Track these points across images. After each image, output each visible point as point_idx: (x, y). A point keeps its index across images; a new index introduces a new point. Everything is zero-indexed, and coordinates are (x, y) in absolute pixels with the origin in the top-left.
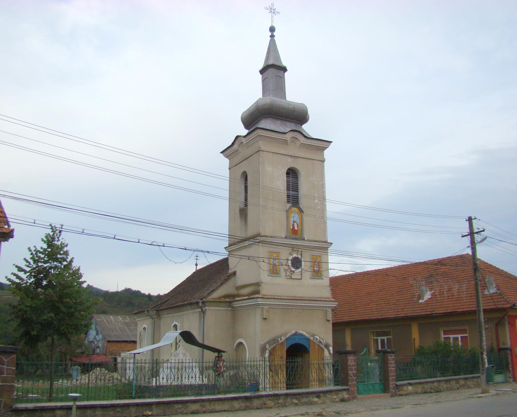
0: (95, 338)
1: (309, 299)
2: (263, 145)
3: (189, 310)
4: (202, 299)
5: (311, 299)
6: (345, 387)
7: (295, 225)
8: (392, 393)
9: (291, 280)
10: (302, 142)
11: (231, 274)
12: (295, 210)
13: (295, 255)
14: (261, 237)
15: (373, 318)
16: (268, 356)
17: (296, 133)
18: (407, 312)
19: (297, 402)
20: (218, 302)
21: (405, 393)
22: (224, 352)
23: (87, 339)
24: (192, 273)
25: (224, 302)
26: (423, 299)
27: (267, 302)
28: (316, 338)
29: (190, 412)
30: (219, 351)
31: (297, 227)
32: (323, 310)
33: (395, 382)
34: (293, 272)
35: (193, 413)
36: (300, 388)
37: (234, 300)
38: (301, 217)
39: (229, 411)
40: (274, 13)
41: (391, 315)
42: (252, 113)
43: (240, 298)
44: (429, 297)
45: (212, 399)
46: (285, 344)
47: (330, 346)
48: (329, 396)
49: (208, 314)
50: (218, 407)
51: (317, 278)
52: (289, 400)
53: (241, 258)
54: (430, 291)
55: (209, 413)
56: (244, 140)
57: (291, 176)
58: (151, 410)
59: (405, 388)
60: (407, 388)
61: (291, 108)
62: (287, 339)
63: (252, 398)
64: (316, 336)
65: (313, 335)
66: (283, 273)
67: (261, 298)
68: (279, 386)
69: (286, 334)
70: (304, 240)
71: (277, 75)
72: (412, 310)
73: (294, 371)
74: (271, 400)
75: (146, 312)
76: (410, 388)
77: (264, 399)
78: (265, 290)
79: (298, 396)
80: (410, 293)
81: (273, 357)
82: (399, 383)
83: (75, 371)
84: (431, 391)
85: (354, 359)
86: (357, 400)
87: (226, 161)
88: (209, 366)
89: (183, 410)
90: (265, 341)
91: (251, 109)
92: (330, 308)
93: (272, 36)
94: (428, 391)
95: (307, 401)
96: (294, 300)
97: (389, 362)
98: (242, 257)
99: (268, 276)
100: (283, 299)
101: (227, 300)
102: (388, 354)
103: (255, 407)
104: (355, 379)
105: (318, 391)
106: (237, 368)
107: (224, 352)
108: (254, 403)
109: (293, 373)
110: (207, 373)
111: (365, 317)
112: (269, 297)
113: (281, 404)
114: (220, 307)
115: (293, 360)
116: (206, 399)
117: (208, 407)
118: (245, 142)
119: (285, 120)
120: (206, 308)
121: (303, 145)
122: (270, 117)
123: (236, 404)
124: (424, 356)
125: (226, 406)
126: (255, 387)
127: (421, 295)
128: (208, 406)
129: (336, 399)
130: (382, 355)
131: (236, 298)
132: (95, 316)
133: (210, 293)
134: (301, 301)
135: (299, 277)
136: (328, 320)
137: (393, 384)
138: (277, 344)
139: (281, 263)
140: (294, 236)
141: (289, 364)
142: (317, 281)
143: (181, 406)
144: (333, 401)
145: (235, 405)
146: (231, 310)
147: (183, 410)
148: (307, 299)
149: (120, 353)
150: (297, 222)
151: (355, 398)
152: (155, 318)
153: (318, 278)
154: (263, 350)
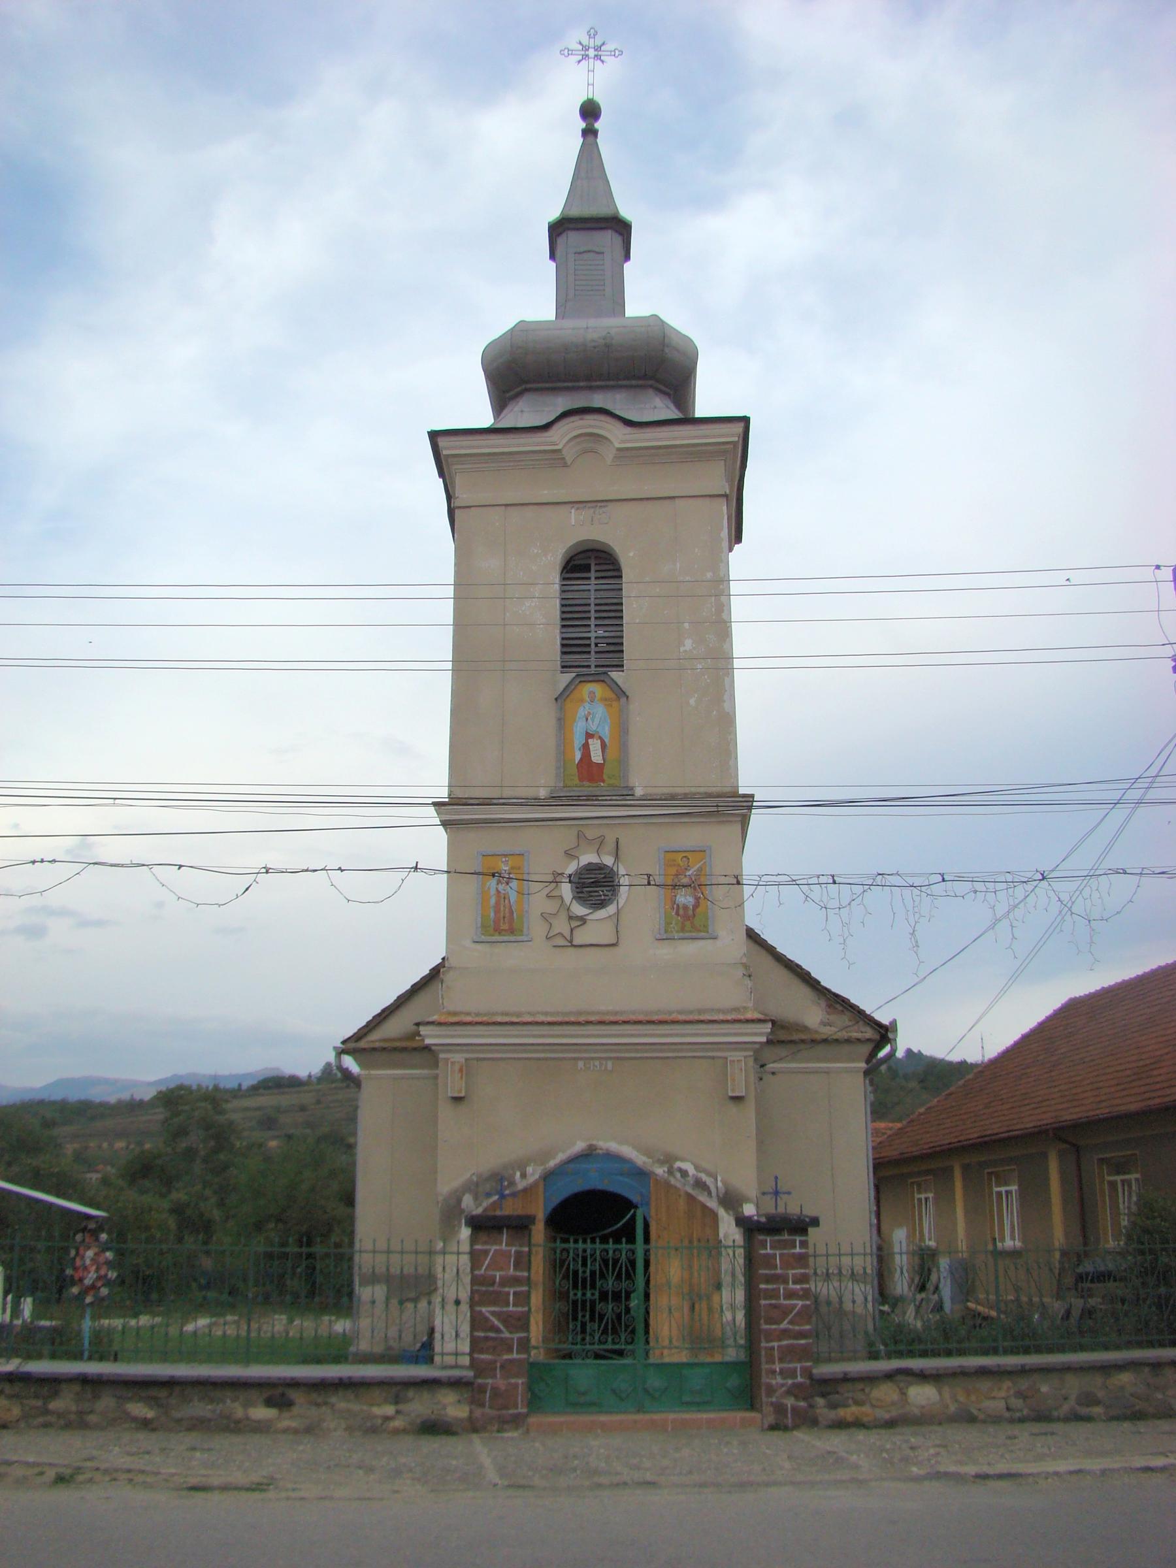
5: (655, 1018)
8: (780, 1409)
9: (572, 950)
10: (617, 445)
13: (588, 858)
17: (596, 417)
19: (150, 1414)
20: (404, 1049)
27: (453, 1036)
28: (680, 1170)
32: (713, 1058)
34: (583, 920)
47: (748, 1200)
48: (341, 1402)
51: (687, 935)
52: (107, 1402)
61: (593, 341)
62: (548, 1177)
64: (683, 1160)
65: (668, 1159)
66: (537, 929)
76: (922, 1395)
79: (163, 1393)
84: (1083, 1411)
85: (518, 1253)
92: (745, 1050)
95: (209, 1415)
99: (474, 942)
113: (60, 1415)
114: (413, 1067)
119: (590, 388)
121: (625, 455)
129: (387, 1418)
136: (737, 1099)
140: (588, 789)
142: (690, 949)
151: (516, 1421)
153: (694, 934)
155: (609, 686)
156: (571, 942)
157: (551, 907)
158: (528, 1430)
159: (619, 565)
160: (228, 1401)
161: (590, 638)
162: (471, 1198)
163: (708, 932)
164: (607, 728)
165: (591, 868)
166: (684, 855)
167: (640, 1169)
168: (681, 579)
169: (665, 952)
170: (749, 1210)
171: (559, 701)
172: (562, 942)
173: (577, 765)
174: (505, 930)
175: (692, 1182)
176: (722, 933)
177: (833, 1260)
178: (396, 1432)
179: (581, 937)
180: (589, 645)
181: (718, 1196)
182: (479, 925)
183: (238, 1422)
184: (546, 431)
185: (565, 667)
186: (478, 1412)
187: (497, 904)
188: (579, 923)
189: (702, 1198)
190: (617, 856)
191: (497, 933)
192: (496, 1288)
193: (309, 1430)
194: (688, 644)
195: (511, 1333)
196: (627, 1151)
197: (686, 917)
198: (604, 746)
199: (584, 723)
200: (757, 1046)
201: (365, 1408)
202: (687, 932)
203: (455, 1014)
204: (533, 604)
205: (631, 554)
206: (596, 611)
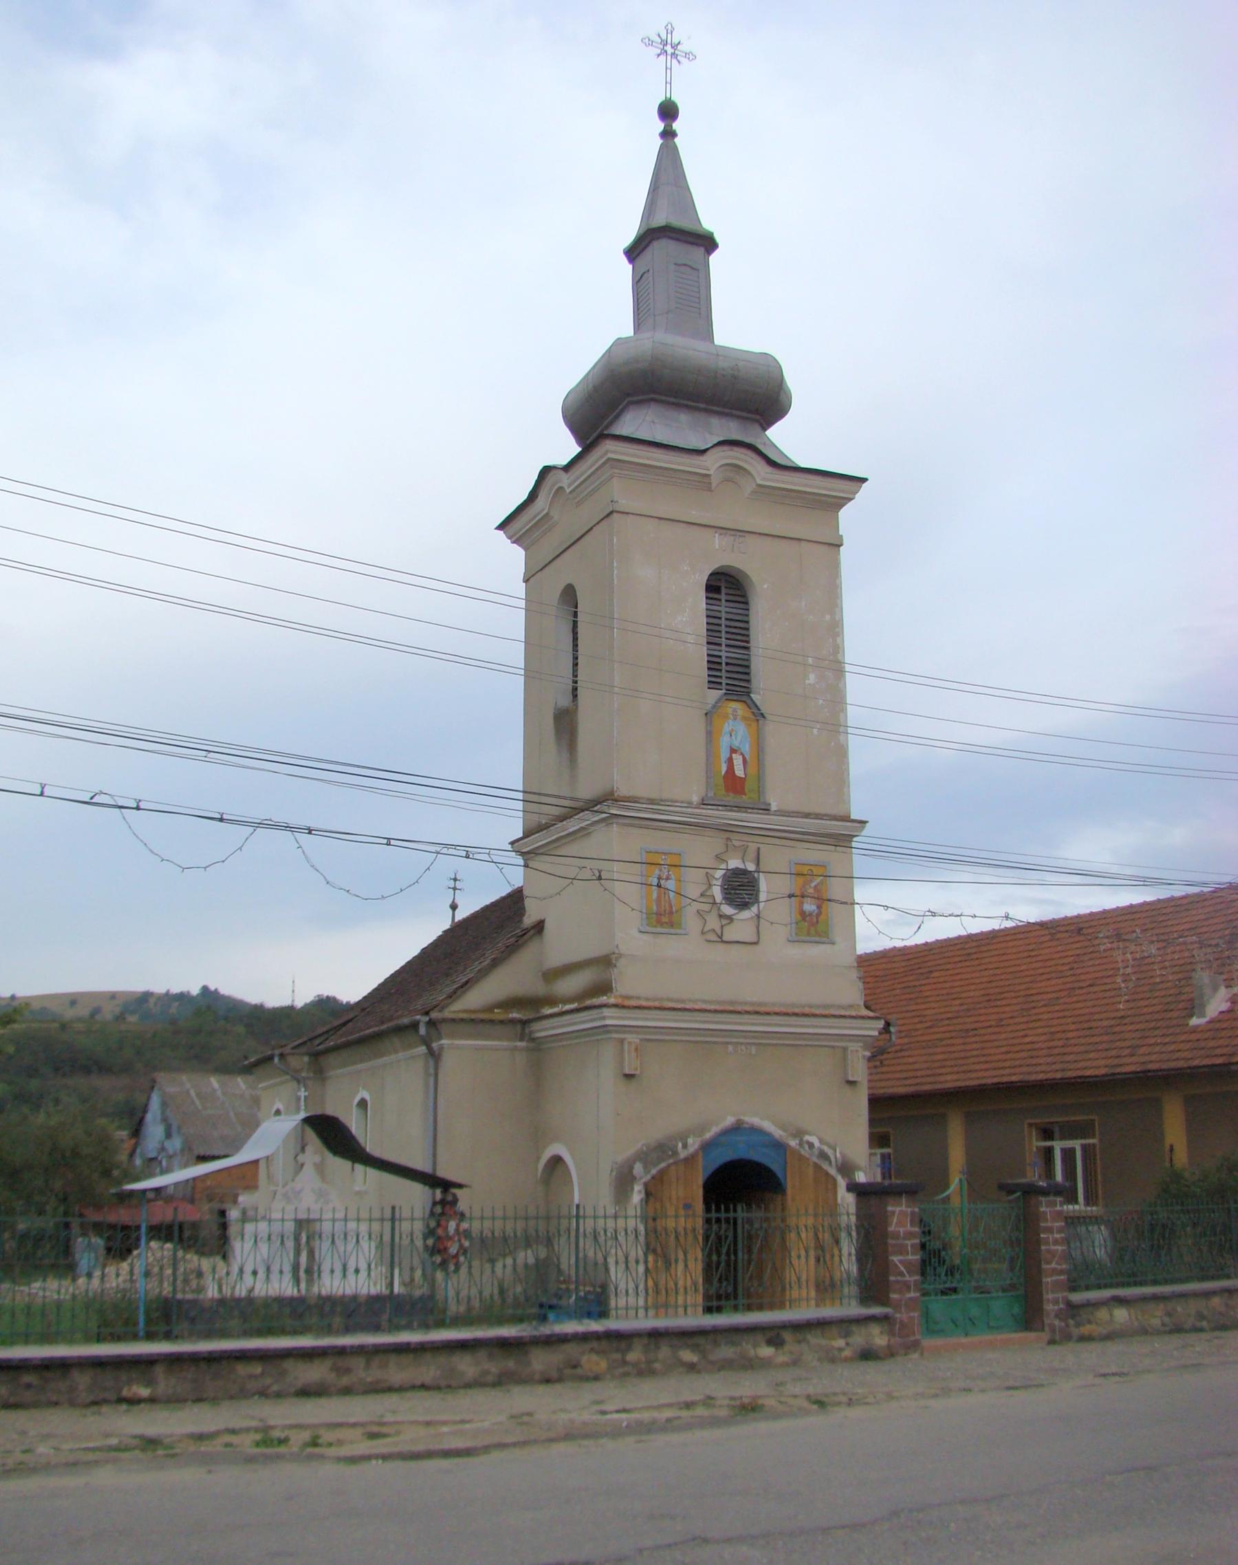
0: (163, 1149)
1: (783, 1010)
2: (622, 493)
3: (396, 1052)
4: (427, 1013)
6: (877, 1310)
7: (738, 761)
8: (1053, 1330)
10: (759, 482)
11: (526, 932)
12: (735, 710)
13: (734, 863)
14: (617, 801)
15: (1033, 1077)
16: (642, 1200)
18: (1147, 1058)
21: (1103, 1331)
22: (460, 1186)
23: (138, 1151)
24: (440, 933)
25: (502, 1022)
26: (1202, 1015)
30: (446, 1185)
32: (833, 1047)
33: (1065, 1294)
34: (730, 918)
36: (760, 1308)
37: (538, 1015)
38: (758, 731)
39: (438, 1388)
40: (674, 55)
41: (1096, 1067)
42: (596, 389)
43: (555, 1010)
44: (1224, 1006)
46: (700, 1160)
47: (859, 1169)
48: (815, 1339)
49: (449, 1062)
50: (396, 1372)
51: (813, 939)
52: (664, 1352)
53: (438, 853)
54: (1227, 987)
56: (565, 480)
57: (723, 597)
58: (150, 1383)
59: (1102, 1314)
60: (1111, 1315)
61: (723, 369)
62: (707, 1147)
64: (810, 1134)
65: (799, 1133)
66: (691, 922)
67: (616, 1006)
68: (680, 1300)
69: (701, 1129)
70: (767, 810)
71: (680, 262)
72: (1163, 1050)
74: (597, 1353)
75: (276, 1060)
76: (1121, 1315)
77: (571, 1349)
78: (629, 982)
79: (701, 1340)
80: (1163, 993)
81: (658, 1207)
82: (1076, 1297)
83: (87, 1250)
84: (1198, 1324)
86: (922, 1354)
87: (517, 554)
90: (630, 1152)
91: (590, 376)
92: (858, 1041)
93: (668, 134)
94: (1187, 1326)
97: (1043, 1224)
98: (445, 851)
99: (641, 932)
102: (1040, 1198)
103: (537, 1377)
104: (915, 1281)
106: (549, 1242)
107: (460, 1186)
109: (723, 1257)
111: (1010, 1075)
112: (644, 1003)
113: (635, 1365)
116: (352, 1347)
117: (362, 1374)
118: (569, 486)
119: (706, 411)
120: (443, 1042)
123: (466, 1365)
124: (1182, 1204)
125: (429, 1370)
126: (598, 1305)
127: (1197, 1002)
128: (361, 1372)
129: (840, 1350)
130: (1019, 1197)
131: (543, 1007)
132: (161, 1077)
133: (455, 992)
134: (755, 1017)
135: (749, 935)
136: (852, 1083)
137: (1056, 1302)
138: (671, 1161)
139: (597, 874)
140: (731, 799)
141: (715, 1227)
142: (815, 951)
144: (832, 1358)
147: (268, 1381)
148: (777, 1009)
149: (236, 1196)
151: (915, 1346)
152: (308, 1078)
153: (817, 939)
154: (623, 1181)
159: (745, 591)
160: (744, 1344)
161: (720, 657)
164: (747, 746)
167: (778, 1142)
170: (861, 1177)
172: (713, 937)
173: (724, 777)
174: (666, 923)
177: (601, 1222)
178: (846, 1360)
179: (731, 933)
180: (720, 663)
181: (837, 1165)
186: (892, 1341)
189: (825, 1166)
190: (758, 864)
192: (900, 1242)
193: (795, 1363)
194: (812, 678)
196: (767, 1126)
197: (812, 924)
199: (729, 739)
204: (684, 619)
205: (765, 586)
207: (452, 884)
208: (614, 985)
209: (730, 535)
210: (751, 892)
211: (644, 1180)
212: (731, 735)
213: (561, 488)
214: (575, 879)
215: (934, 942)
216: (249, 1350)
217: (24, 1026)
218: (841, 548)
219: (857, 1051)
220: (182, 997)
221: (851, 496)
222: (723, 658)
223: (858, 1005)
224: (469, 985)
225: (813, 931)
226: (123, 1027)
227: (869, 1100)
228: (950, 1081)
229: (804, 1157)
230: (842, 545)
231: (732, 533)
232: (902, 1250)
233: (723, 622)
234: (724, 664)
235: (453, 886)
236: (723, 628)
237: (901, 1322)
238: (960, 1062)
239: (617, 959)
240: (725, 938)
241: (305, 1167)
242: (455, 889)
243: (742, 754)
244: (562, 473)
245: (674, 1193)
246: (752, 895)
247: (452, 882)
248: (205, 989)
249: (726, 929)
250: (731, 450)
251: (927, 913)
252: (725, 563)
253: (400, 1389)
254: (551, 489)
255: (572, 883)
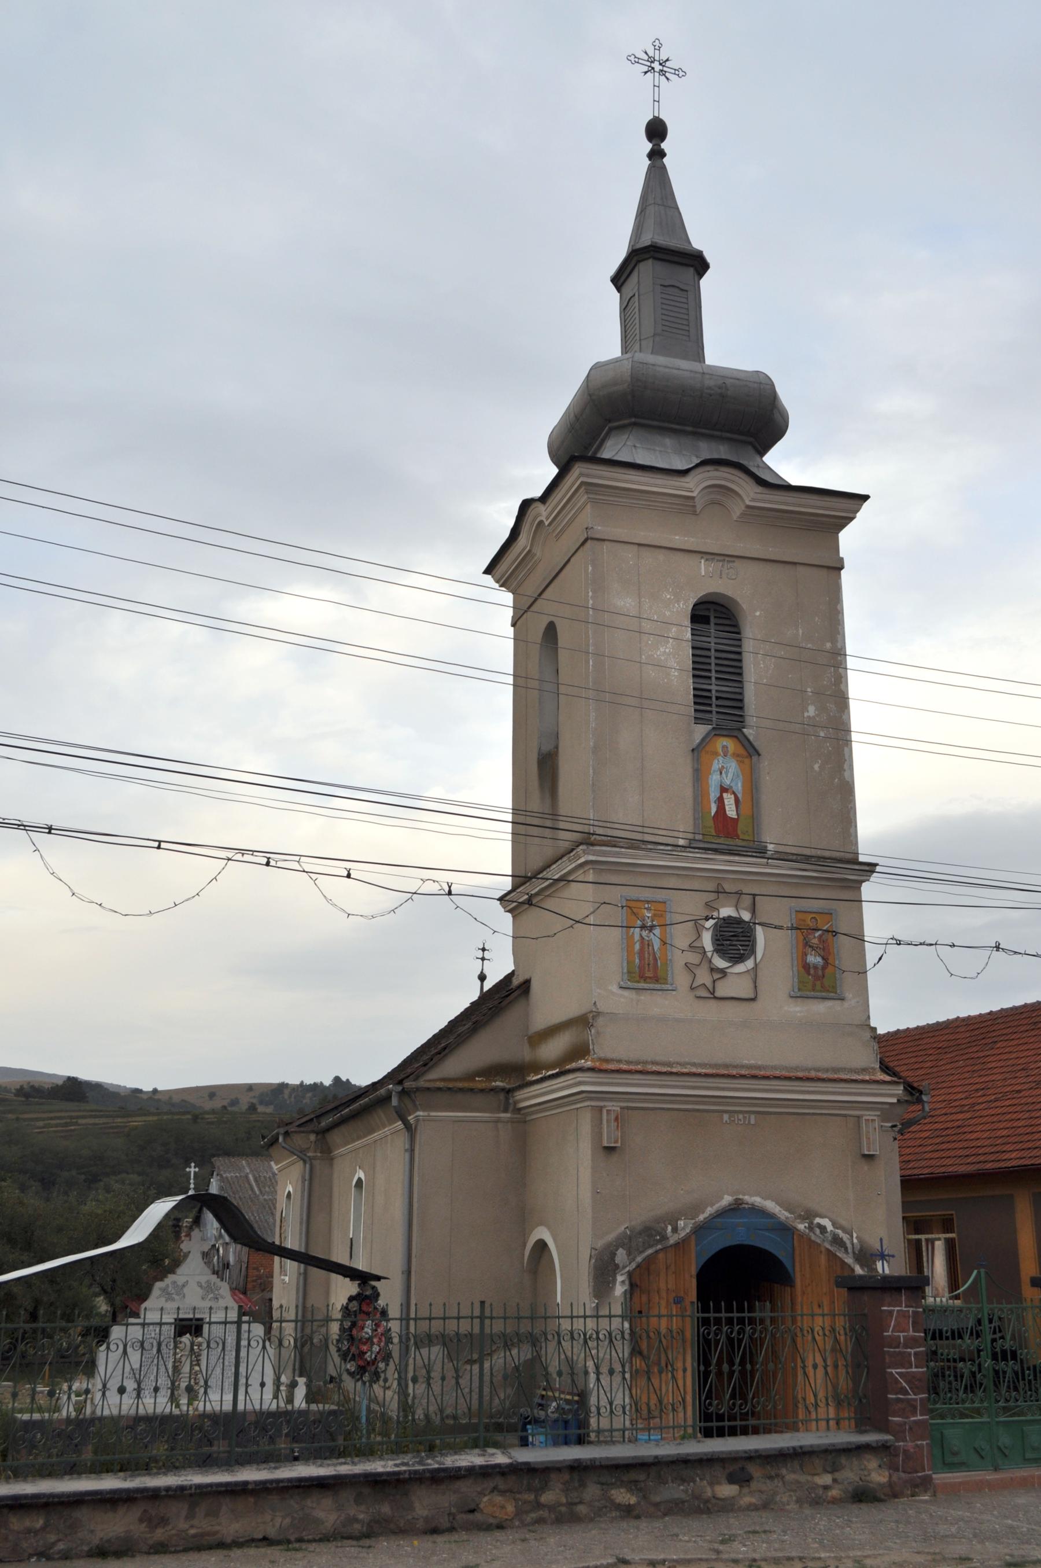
1: (785, 1073)
4: (400, 1082)
6: (871, 1438)
7: (729, 800)
9: (713, 1004)
10: (748, 503)
13: (726, 912)
19: (633, 1500)
22: (378, 1278)
25: (482, 1091)
28: (819, 1226)
29: (86, 1548)
30: (363, 1278)
31: (734, 807)
32: (845, 1116)
34: (723, 972)
35: (101, 1552)
42: (577, 418)
45: (199, 1486)
48: (791, 1475)
52: (592, 1491)
53: (229, 859)
55: (186, 1550)
61: (710, 388)
62: (700, 1230)
63: (405, 1482)
64: (822, 1217)
65: (809, 1215)
66: (681, 979)
69: (696, 1208)
70: (761, 852)
73: (737, 1360)
74: (502, 1493)
75: (281, 1139)
77: (466, 1487)
79: (642, 1477)
86: (934, 1495)
88: (457, 1334)
89: (52, 1538)
90: (610, 1237)
93: (657, 155)
95: (683, 1496)
96: (723, 1076)
100: (676, 1074)
101: (498, 1083)
103: (420, 1524)
105: (737, 1452)
106: (534, 1341)
107: (378, 1278)
108: (417, 1505)
110: (418, 1357)
112: (624, 1067)
113: (551, 1508)
115: (746, 1314)
116: (168, 1489)
117: (183, 1525)
118: (547, 519)
119: (694, 434)
122: (635, 424)
129: (826, 1488)
135: (746, 992)
136: (869, 1158)
138: (659, 1247)
142: (820, 1008)
143: (40, 1523)
144: (816, 1500)
145: (320, 1514)
146: (511, 1121)
147: (52, 1538)
150: (735, 789)
151: (925, 1484)
152: (315, 1158)
153: (824, 994)
155: (740, 742)
156: (713, 993)
157: (694, 958)
158: (935, 1492)
161: (710, 691)
162: (625, 1252)
163: (836, 993)
164: (740, 785)
165: (728, 921)
166: (813, 915)
168: (804, 645)
169: (798, 1010)
171: (696, 752)
172: (704, 993)
174: (650, 978)
175: (830, 1238)
176: (848, 995)
178: (834, 1501)
180: (710, 698)
181: (854, 1253)
182: (625, 971)
183: (707, 1501)
184: (684, 476)
185: (698, 720)
187: (641, 951)
188: (719, 976)
191: (642, 981)
193: (765, 1506)
194: (811, 711)
195: (915, 1395)
196: (771, 1206)
197: (817, 978)
198: (737, 801)
200: (887, 1106)
201: (809, 1478)
202: (818, 991)
203: (607, 1061)
204: (667, 650)
205: (758, 614)
206: (710, 664)
207: (480, 954)
208: (591, 1047)
209: (718, 561)
210: (747, 943)
211: (627, 1269)
212: (721, 773)
213: (541, 522)
214: (415, 893)
215: (999, 1011)
216: (26, 1496)
217: (155, 1118)
218: (842, 572)
219: (873, 1120)
220: (316, 1087)
221: (851, 515)
222: (714, 692)
223: (874, 1069)
224: (447, 1051)
225: (818, 987)
226: (254, 1117)
227: (902, 1181)
228: (1013, 1159)
229: (814, 1242)
230: (842, 568)
231: (722, 558)
232: (903, 1361)
233: (713, 653)
234: (714, 699)
235: (481, 956)
236: (713, 661)
237: (905, 1451)
238: (1026, 1138)
239: (594, 1018)
240: (717, 994)
241: (191, 1256)
242: (483, 959)
243: (734, 793)
244: (539, 504)
245: (663, 1286)
246: (748, 946)
247: (486, 957)
248: (337, 1079)
249: (719, 984)
250: (717, 470)
251: (891, 941)
252: (712, 589)
253: (237, 1544)
254: (532, 524)
255: (411, 898)
